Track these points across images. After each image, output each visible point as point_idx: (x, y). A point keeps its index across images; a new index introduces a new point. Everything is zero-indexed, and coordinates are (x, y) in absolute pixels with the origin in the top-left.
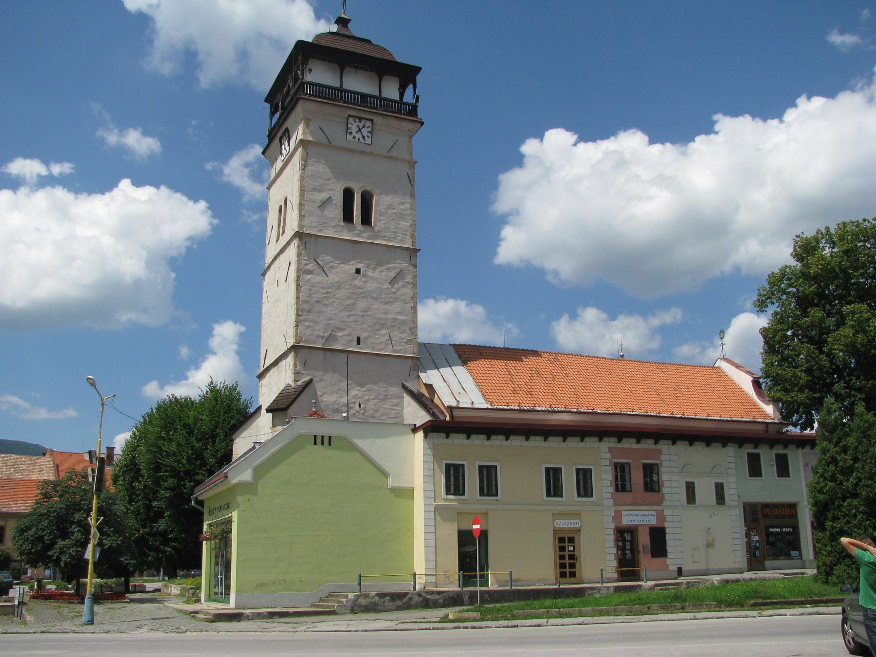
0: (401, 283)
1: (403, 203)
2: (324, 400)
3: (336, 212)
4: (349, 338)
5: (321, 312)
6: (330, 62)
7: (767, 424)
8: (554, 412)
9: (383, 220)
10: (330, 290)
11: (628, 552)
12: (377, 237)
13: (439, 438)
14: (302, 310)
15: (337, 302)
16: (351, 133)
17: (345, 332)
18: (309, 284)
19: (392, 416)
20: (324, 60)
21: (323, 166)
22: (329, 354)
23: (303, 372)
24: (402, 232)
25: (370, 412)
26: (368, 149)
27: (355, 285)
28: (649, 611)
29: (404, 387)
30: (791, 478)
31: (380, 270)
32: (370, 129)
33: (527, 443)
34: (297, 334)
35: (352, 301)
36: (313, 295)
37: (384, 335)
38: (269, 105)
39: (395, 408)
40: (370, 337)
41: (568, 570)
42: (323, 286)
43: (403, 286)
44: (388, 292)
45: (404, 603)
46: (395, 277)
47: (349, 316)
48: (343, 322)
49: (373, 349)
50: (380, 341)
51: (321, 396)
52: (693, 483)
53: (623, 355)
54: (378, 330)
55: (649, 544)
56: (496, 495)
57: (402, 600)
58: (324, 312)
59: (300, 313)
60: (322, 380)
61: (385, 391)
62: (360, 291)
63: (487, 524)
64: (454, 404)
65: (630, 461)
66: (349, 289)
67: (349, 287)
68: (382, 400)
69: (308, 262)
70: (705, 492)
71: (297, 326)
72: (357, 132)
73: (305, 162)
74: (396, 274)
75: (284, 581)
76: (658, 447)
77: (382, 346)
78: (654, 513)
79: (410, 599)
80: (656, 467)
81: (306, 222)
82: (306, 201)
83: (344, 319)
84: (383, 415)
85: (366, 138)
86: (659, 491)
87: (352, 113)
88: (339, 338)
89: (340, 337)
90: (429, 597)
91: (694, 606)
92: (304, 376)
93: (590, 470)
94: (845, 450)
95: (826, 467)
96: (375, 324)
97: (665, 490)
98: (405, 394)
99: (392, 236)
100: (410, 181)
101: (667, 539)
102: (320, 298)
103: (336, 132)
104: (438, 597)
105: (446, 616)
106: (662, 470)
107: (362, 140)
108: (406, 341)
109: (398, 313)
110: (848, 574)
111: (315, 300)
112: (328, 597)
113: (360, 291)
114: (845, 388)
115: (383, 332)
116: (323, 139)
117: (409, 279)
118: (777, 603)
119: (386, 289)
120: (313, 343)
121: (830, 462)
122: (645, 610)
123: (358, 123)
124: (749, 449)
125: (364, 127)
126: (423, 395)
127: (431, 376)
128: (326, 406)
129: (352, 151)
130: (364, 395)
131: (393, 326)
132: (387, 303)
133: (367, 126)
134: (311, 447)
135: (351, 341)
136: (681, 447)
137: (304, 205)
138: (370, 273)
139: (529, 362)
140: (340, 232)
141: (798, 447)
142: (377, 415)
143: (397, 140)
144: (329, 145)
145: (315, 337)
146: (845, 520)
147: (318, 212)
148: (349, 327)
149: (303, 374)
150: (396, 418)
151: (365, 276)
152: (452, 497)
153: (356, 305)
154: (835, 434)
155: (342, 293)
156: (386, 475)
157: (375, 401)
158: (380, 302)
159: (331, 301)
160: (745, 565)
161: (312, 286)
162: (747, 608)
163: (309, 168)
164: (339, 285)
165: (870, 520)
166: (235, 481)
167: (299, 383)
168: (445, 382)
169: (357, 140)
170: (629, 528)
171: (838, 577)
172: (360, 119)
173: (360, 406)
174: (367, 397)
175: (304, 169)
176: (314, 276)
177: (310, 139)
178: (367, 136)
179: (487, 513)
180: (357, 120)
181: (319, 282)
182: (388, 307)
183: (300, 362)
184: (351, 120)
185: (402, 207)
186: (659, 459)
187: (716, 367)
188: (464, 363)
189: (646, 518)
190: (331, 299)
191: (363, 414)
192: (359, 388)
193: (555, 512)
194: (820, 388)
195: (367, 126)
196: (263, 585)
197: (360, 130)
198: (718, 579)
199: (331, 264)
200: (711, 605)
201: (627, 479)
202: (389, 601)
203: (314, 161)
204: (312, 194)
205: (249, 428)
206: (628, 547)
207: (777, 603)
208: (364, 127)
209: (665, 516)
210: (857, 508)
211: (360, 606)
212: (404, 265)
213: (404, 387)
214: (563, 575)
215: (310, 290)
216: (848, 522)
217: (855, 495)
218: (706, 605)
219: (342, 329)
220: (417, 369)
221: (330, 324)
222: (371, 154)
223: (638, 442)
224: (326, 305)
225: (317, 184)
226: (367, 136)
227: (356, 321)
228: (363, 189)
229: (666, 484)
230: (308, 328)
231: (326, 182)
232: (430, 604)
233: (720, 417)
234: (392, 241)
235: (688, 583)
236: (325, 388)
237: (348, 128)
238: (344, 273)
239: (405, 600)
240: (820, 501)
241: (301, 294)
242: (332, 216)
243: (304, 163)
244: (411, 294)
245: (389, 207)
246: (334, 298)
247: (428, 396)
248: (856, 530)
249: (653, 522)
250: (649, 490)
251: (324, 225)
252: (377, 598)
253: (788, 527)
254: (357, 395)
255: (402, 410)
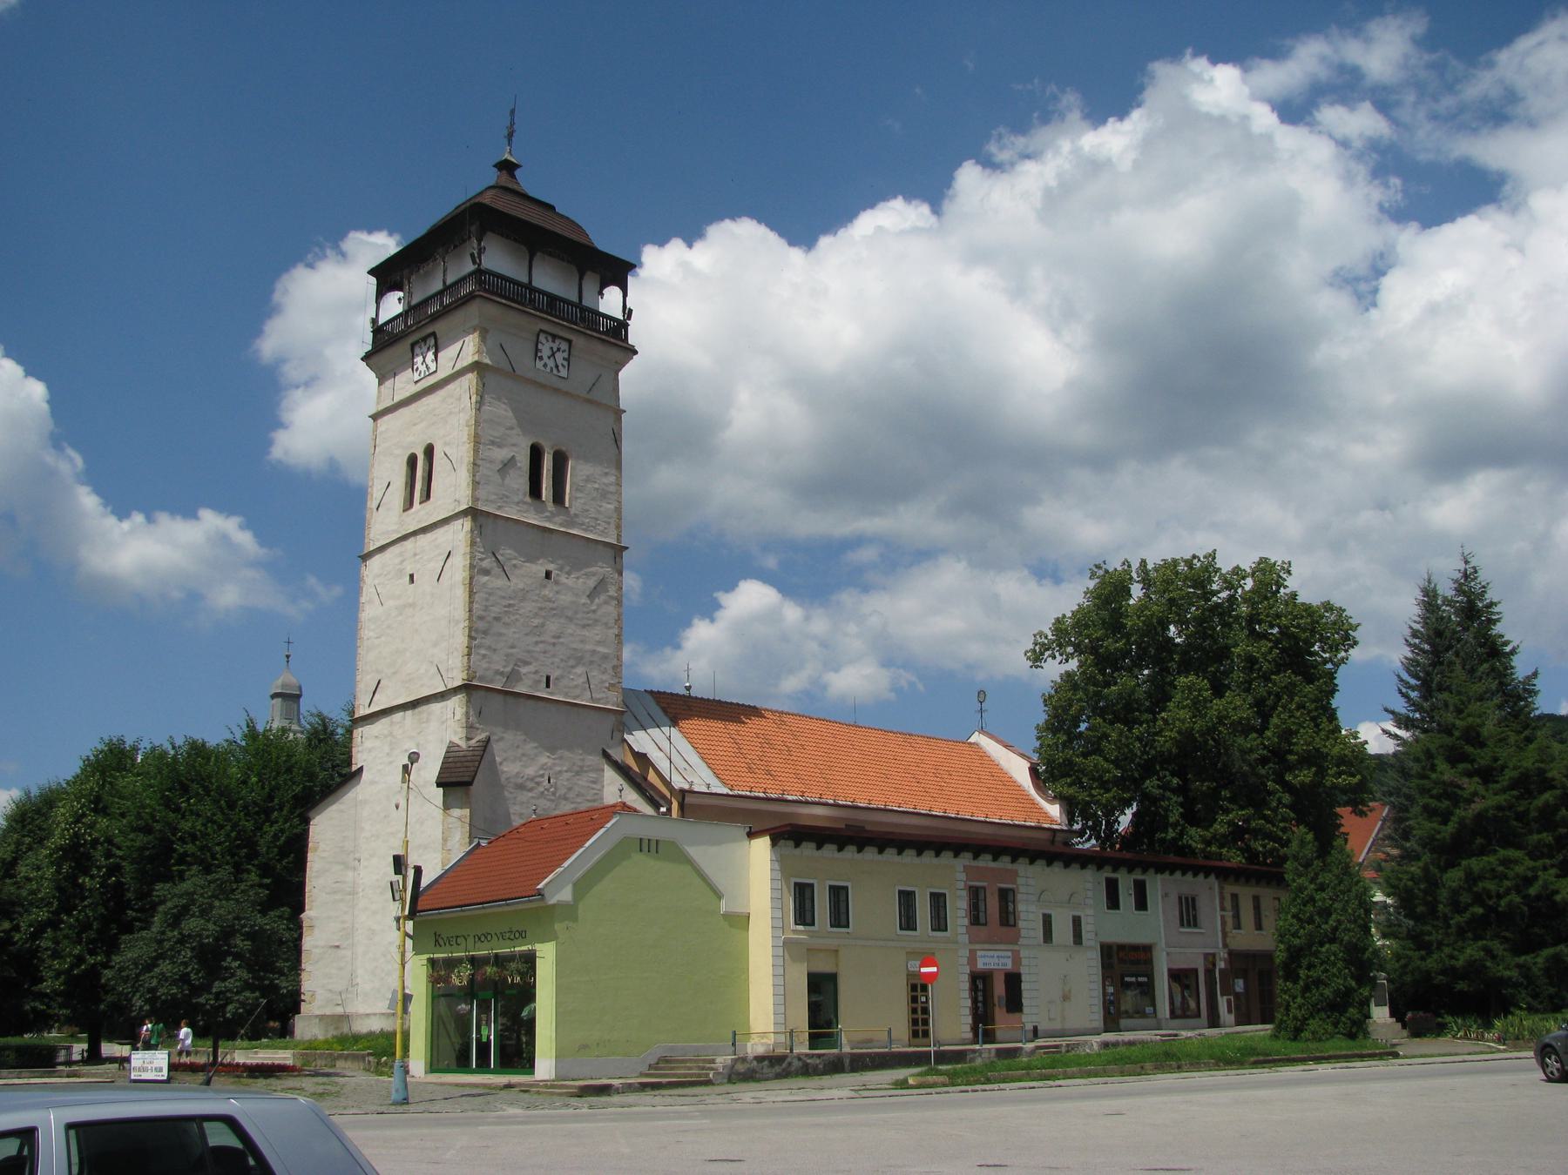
0: (603, 597)
1: (606, 474)
2: (505, 769)
3: (519, 481)
4: (537, 677)
5: (501, 634)
6: (515, 240)
7: (1054, 831)
8: (807, 803)
9: (580, 498)
10: (511, 602)
11: (980, 1005)
12: (572, 524)
13: (787, 847)
14: (476, 631)
15: (522, 620)
16: (541, 358)
17: (531, 668)
18: (485, 590)
19: (589, 798)
20: (508, 237)
21: (504, 406)
22: (510, 700)
23: (477, 725)
24: (605, 519)
25: (562, 791)
26: (561, 385)
27: (545, 596)
28: (1141, 1072)
29: (606, 755)
30: (1149, 912)
31: (576, 576)
32: (566, 354)
33: (880, 857)
34: (470, 667)
35: (541, 621)
36: (491, 608)
37: (580, 676)
38: (375, 279)
39: (594, 786)
40: (562, 677)
41: (920, 1028)
42: (503, 594)
43: (606, 603)
44: (586, 610)
45: (784, 1070)
46: (595, 588)
47: (537, 643)
48: (528, 652)
49: (566, 695)
50: (575, 683)
51: (501, 764)
52: (1079, 917)
53: (690, 687)
54: (573, 667)
55: (1004, 994)
56: (847, 926)
57: (781, 1065)
58: (504, 634)
59: (473, 634)
60: (501, 739)
61: (580, 759)
62: (551, 605)
63: (837, 965)
64: (686, 787)
65: (985, 884)
66: (536, 601)
67: (536, 598)
68: (577, 773)
69: (484, 556)
70: (1063, 930)
71: (469, 654)
72: (549, 358)
73: (481, 397)
74: (596, 583)
75: (609, 1041)
76: (1015, 866)
77: (578, 692)
78: (1009, 954)
79: (790, 1064)
80: (983, 891)
81: (482, 493)
82: (482, 459)
83: (530, 648)
84: (577, 795)
85: (560, 367)
86: (1015, 926)
87: (545, 327)
88: (523, 677)
89: (524, 674)
90: (809, 1061)
91: (1191, 1064)
92: (479, 731)
93: (913, 893)
94: (1322, 888)
95: (1302, 907)
96: (569, 658)
97: (1021, 924)
98: (606, 766)
99: (591, 524)
100: (616, 441)
101: (1023, 988)
102: (500, 613)
103: (520, 353)
104: (818, 1061)
105: (905, 1081)
106: (1019, 897)
107: (555, 371)
108: (607, 685)
109: (599, 643)
110: (1324, 1029)
111: (493, 615)
112: (657, 1064)
113: (551, 605)
114: (1159, 787)
115: (580, 670)
116: (505, 365)
117: (612, 592)
118: (1280, 1060)
119: (584, 604)
120: (491, 681)
121: (1308, 902)
122: (1139, 1070)
123: (551, 344)
124: (1107, 873)
125: (559, 350)
126: (630, 768)
127: (641, 740)
128: (507, 779)
129: (543, 386)
130: (554, 765)
131: (591, 662)
132: (584, 626)
133: (562, 349)
134: (638, 857)
135: (539, 681)
136: (1039, 867)
137: (479, 466)
138: (563, 579)
139: (754, 724)
140: (525, 512)
141: (1156, 873)
142: (571, 795)
143: (600, 376)
144: (512, 374)
145: (493, 673)
146: (1322, 968)
147: (497, 478)
148: (537, 659)
149: (478, 729)
150: (594, 801)
151: (557, 583)
152: (801, 928)
153: (546, 627)
154: (1310, 869)
155: (528, 607)
156: (719, 896)
157: (569, 774)
158: (576, 624)
159: (513, 618)
160: (1099, 1023)
161: (490, 594)
162: (1247, 1066)
163: (486, 408)
164: (523, 595)
165: (1348, 968)
166: (552, 901)
167: (473, 742)
168: (661, 750)
169: (548, 370)
170: (984, 973)
171: (1313, 1033)
172: (554, 337)
173: (549, 781)
174: (558, 769)
175: (479, 410)
176: (493, 579)
177: (487, 361)
178: (563, 365)
179: (837, 951)
180: (550, 338)
181: (498, 588)
182: (585, 632)
183: (474, 710)
184: (542, 338)
185: (605, 480)
186: (1015, 883)
187: (970, 743)
188: (674, 722)
189: (1002, 960)
190: (513, 615)
191: (554, 794)
192: (548, 754)
193: (909, 950)
194: (1293, 819)
195: (562, 349)
196: (585, 1047)
197: (553, 355)
198: (1098, 1040)
199: (514, 562)
200: (1209, 1063)
201: (982, 908)
202: (768, 1067)
203: (492, 398)
204: (489, 449)
205: (341, 801)
206: (980, 998)
207: (1280, 1060)
208: (559, 350)
209: (1020, 958)
210: (1335, 954)
211: (739, 1074)
212: (603, 569)
213: (606, 755)
214: (915, 1034)
215: (487, 600)
216: (1326, 971)
217: (1332, 940)
218: (1204, 1063)
219: (527, 663)
220: (622, 728)
221: (512, 655)
222: (567, 394)
223: (995, 859)
224: (506, 625)
225: (496, 434)
226: (563, 365)
227: (545, 652)
228: (554, 449)
229: (1023, 916)
230: (483, 659)
231: (508, 432)
232: (810, 1071)
233: (1000, 819)
234: (591, 531)
235: (1068, 1045)
236: (505, 752)
237: (537, 350)
238: (531, 577)
239: (784, 1065)
240: (1295, 946)
241: (475, 606)
242: (516, 486)
243: (479, 399)
244: (615, 615)
245: (588, 480)
246: (518, 614)
247: (638, 770)
248: (1335, 979)
249: (1009, 966)
250: (301, 879)
251: (505, 499)
252: (755, 1063)
253: (1144, 976)
254: (546, 764)
255: (601, 790)
